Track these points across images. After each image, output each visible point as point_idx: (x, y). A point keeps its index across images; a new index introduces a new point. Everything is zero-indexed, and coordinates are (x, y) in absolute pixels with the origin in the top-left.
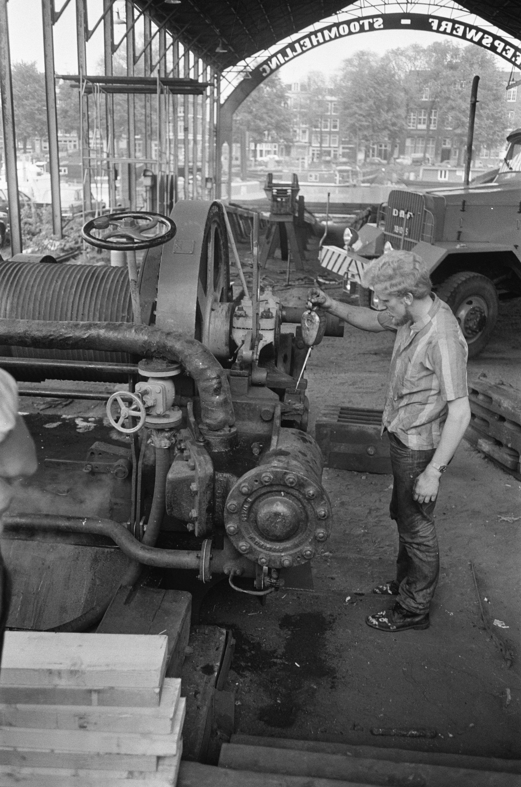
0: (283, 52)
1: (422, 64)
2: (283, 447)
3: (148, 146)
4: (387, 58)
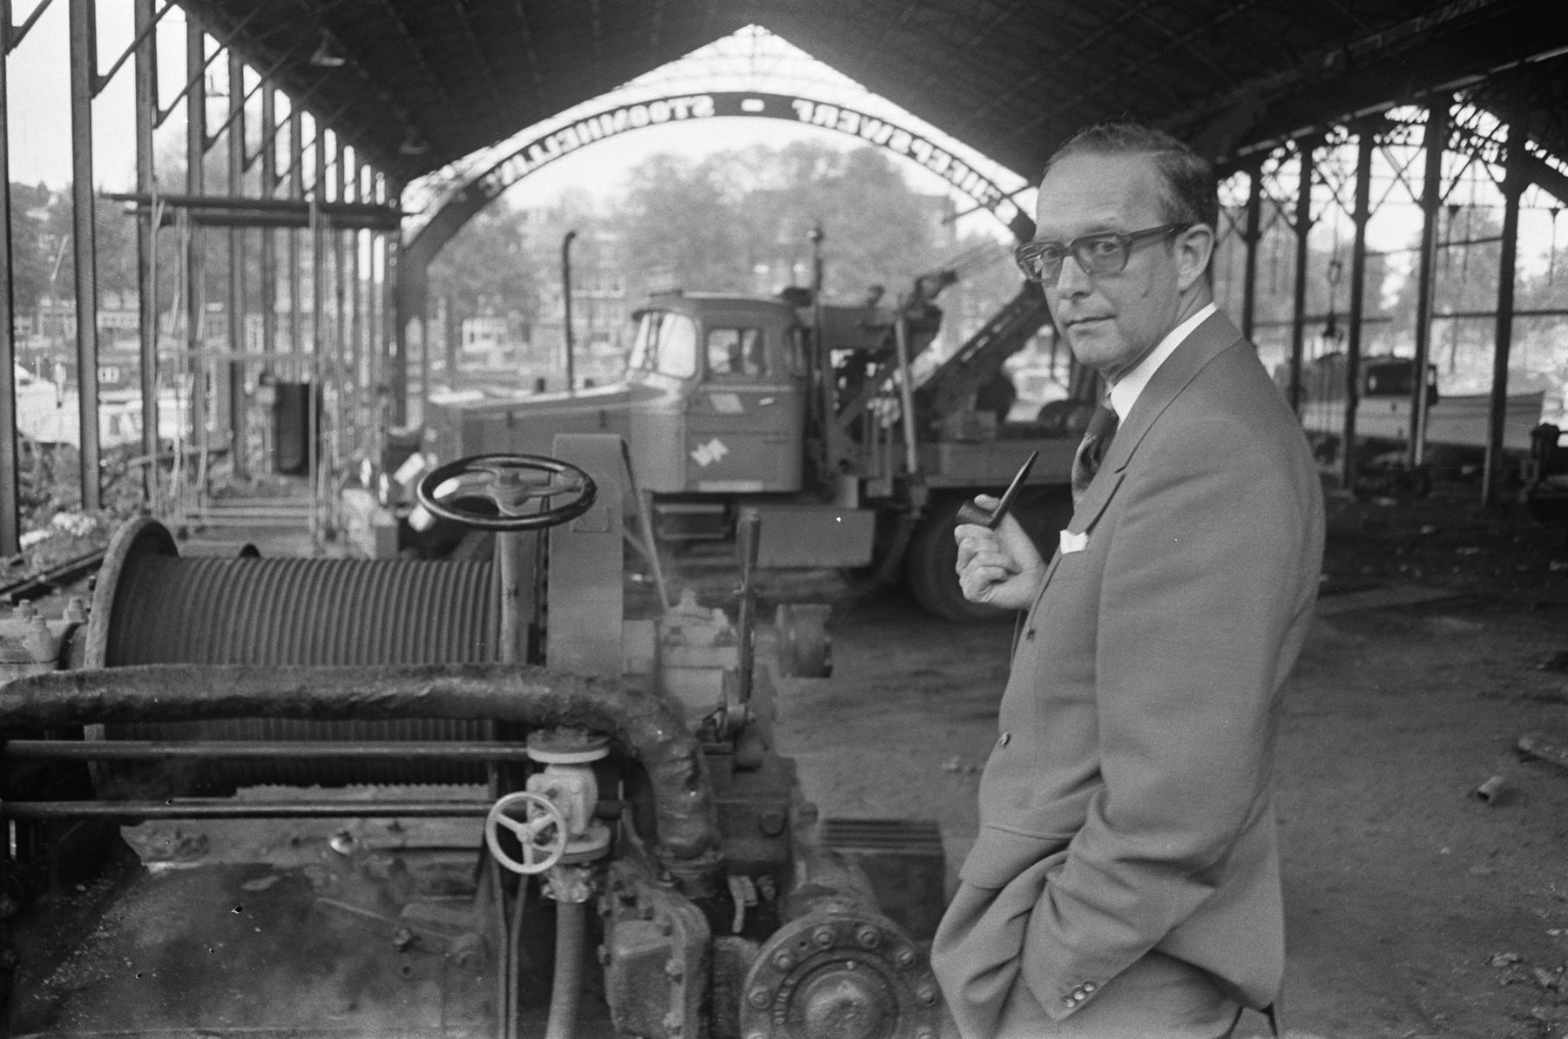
0: (525, 153)
1: (774, 178)
2: (820, 880)
3: (238, 325)
4: (707, 169)
